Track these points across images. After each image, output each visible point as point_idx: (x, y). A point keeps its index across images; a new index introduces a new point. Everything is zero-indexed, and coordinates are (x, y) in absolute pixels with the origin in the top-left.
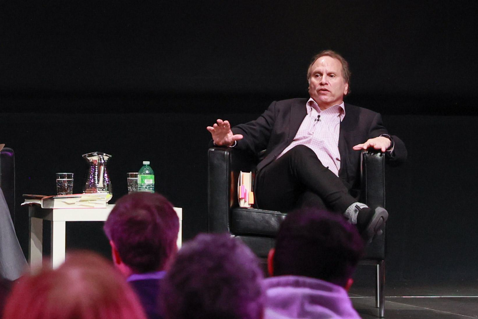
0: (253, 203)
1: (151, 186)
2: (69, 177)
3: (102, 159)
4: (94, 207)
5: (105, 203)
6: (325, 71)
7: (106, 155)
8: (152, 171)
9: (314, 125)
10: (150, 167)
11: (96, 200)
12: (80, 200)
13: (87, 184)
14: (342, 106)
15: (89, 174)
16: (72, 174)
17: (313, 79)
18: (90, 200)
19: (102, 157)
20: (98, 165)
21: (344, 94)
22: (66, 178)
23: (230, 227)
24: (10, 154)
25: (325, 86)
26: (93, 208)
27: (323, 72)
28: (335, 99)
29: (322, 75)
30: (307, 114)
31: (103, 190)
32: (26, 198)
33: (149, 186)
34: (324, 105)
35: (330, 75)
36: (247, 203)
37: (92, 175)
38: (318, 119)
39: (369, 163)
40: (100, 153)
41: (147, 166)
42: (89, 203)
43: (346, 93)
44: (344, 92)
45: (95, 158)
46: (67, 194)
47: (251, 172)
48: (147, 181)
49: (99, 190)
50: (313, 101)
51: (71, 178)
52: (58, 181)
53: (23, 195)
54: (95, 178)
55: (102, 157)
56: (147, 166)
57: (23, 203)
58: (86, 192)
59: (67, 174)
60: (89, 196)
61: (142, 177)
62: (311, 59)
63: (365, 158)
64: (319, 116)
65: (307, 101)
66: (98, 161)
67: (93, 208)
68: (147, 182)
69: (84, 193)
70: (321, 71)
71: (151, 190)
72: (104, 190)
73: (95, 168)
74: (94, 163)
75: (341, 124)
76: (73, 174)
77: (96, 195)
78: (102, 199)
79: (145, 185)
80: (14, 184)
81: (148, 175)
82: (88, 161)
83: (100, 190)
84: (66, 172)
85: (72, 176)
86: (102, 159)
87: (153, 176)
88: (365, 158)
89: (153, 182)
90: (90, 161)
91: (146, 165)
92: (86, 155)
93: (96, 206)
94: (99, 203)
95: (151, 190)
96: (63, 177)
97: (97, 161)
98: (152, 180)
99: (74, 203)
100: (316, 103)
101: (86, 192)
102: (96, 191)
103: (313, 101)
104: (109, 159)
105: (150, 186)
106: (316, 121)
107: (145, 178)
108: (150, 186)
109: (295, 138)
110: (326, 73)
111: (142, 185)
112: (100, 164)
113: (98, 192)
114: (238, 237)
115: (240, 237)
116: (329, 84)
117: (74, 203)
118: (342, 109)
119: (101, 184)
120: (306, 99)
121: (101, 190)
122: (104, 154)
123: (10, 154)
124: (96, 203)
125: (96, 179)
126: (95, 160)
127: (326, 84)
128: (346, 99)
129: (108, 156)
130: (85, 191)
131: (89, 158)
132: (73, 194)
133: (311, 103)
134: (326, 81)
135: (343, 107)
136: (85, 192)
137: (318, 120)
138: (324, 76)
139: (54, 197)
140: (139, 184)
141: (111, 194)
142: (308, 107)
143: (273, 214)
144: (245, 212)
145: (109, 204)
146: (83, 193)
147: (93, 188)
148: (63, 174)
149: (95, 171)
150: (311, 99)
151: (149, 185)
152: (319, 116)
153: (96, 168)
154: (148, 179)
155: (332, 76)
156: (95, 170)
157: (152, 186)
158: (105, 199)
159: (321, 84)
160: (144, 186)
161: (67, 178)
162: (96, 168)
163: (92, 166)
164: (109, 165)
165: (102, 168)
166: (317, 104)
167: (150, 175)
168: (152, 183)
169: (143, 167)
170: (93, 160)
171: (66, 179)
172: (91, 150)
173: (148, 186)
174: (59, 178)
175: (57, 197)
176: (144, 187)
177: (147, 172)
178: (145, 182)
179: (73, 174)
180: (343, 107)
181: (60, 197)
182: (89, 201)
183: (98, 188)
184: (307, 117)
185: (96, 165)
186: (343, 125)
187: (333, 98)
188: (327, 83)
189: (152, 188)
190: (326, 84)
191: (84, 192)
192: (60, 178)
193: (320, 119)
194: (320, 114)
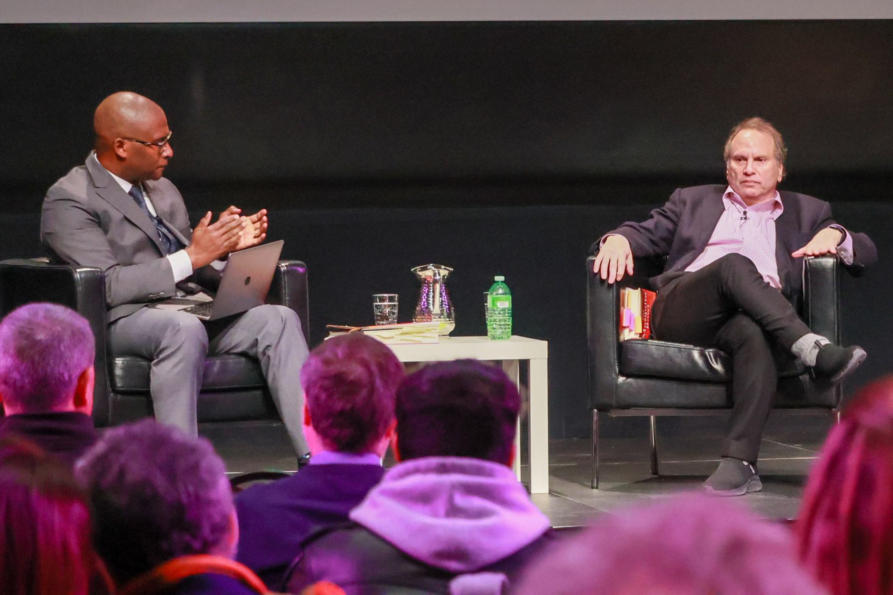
0: (641, 332)
1: (507, 311)
2: (391, 299)
3: (437, 274)
4: (421, 342)
5: (438, 335)
6: (751, 155)
7: (445, 269)
8: (508, 290)
9: (741, 226)
10: (504, 284)
11: (424, 332)
12: (401, 332)
13: (417, 309)
14: (778, 198)
15: (421, 295)
16: (395, 296)
17: (733, 164)
18: (416, 333)
19: (437, 272)
20: (433, 283)
21: (778, 182)
22: (387, 300)
23: (620, 366)
24: (301, 270)
25: (751, 177)
26: (420, 343)
27: (748, 157)
28: (765, 192)
29: (746, 159)
30: (725, 209)
31: (440, 317)
32: (330, 331)
33: (503, 312)
34: (749, 200)
35: (758, 159)
36: (633, 333)
37: (424, 297)
38: (744, 216)
39: (815, 272)
40: (438, 263)
41: (500, 283)
42: (414, 336)
43: (780, 179)
44: (777, 179)
45: (428, 273)
46: (389, 324)
47: (639, 289)
48: (501, 303)
49: (434, 318)
50: (733, 192)
51: (395, 302)
52: (376, 306)
53: (328, 326)
54: (429, 300)
55: (437, 272)
56: (500, 283)
57: (327, 336)
58: (417, 320)
59: (389, 296)
60: (414, 327)
61: (493, 298)
62: (726, 133)
63: (808, 266)
64: (745, 213)
65: (724, 193)
66: (433, 278)
67: (420, 343)
68: (501, 305)
69: (414, 322)
70: (745, 155)
71: (506, 316)
72: (442, 317)
73: (428, 287)
74: (428, 280)
75: (777, 222)
76: (397, 296)
77: (423, 326)
78: (433, 331)
79: (498, 309)
80: (307, 314)
81: (502, 296)
82: (419, 278)
83: (436, 317)
84: (387, 293)
85: (396, 299)
86: (437, 274)
87: (509, 297)
88: (808, 266)
89: (509, 305)
90: (422, 277)
91: (498, 282)
92: (417, 269)
93: (424, 340)
94: (428, 336)
95: (506, 316)
96: (382, 300)
97: (431, 276)
98: (508, 303)
99: (393, 337)
100: (738, 196)
101: (417, 320)
102: (431, 319)
103: (733, 192)
104: (450, 273)
105: (505, 310)
106: (744, 221)
107: (498, 299)
108: (505, 310)
109: (711, 241)
110: (753, 157)
111: (494, 310)
112: (435, 282)
113: (434, 320)
114: (630, 380)
115: (634, 380)
116: (757, 173)
117: (393, 337)
118: (777, 202)
119: (436, 309)
120: (722, 185)
121: (438, 317)
122: (443, 267)
123: (301, 270)
124: (424, 337)
125: (431, 302)
126: (429, 276)
127: (754, 174)
128: (780, 187)
129: (448, 270)
130: (415, 319)
131: (420, 273)
132: (398, 323)
133: (730, 195)
134: (753, 169)
135: (780, 201)
136: (416, 321)
137: (746, 218)
138: (751, 160)
139: (363, 330)
140: (489, 309)
141: (453, 323)
142: (726, 201)
143: (680, 348)
144: (640, 345)
145: (450, 336)
146: (413, 321)
147: (427, 313)
148: (384, 297)
149: (429, 291)
150: (729, 190)
151: (503, 310)
152: (745, 213)
153: (431, 287)
154: (501, 300)
155: (761, 160)
156: (429, 289)
157: (509, 310)
158: (437, 331)
159: (746, 174)
160: (497, 310)
161: (389, 302)
162: (431, 287)
163: (426, 284)
164: (449, 284)
165: (438, 286)
166: (739, 197)
167: (504, 296)
168: (508, 306)
169: (495, 284)
170: (426, 276)
171: (386, 303)
172: (424, 262)
173: (502, 310)
174: (377, 302)
175: (369, 329)
176: (497, 312)
177: (501, 291)
178: (497, 306)
179: (397, 296)
180: (780, 201)
181: (374, 329)
182: (414, 334)
183: (433, 314)
184: (725, 214)
185: (431, 283)
186: (780, 223)
187: (763, 190)
188: (755, 172)
189: (508, 313)
190: (754, 174)
191: (414, 320)
192: (379, 302)
193: (748, 215)
194: (746, 210)
